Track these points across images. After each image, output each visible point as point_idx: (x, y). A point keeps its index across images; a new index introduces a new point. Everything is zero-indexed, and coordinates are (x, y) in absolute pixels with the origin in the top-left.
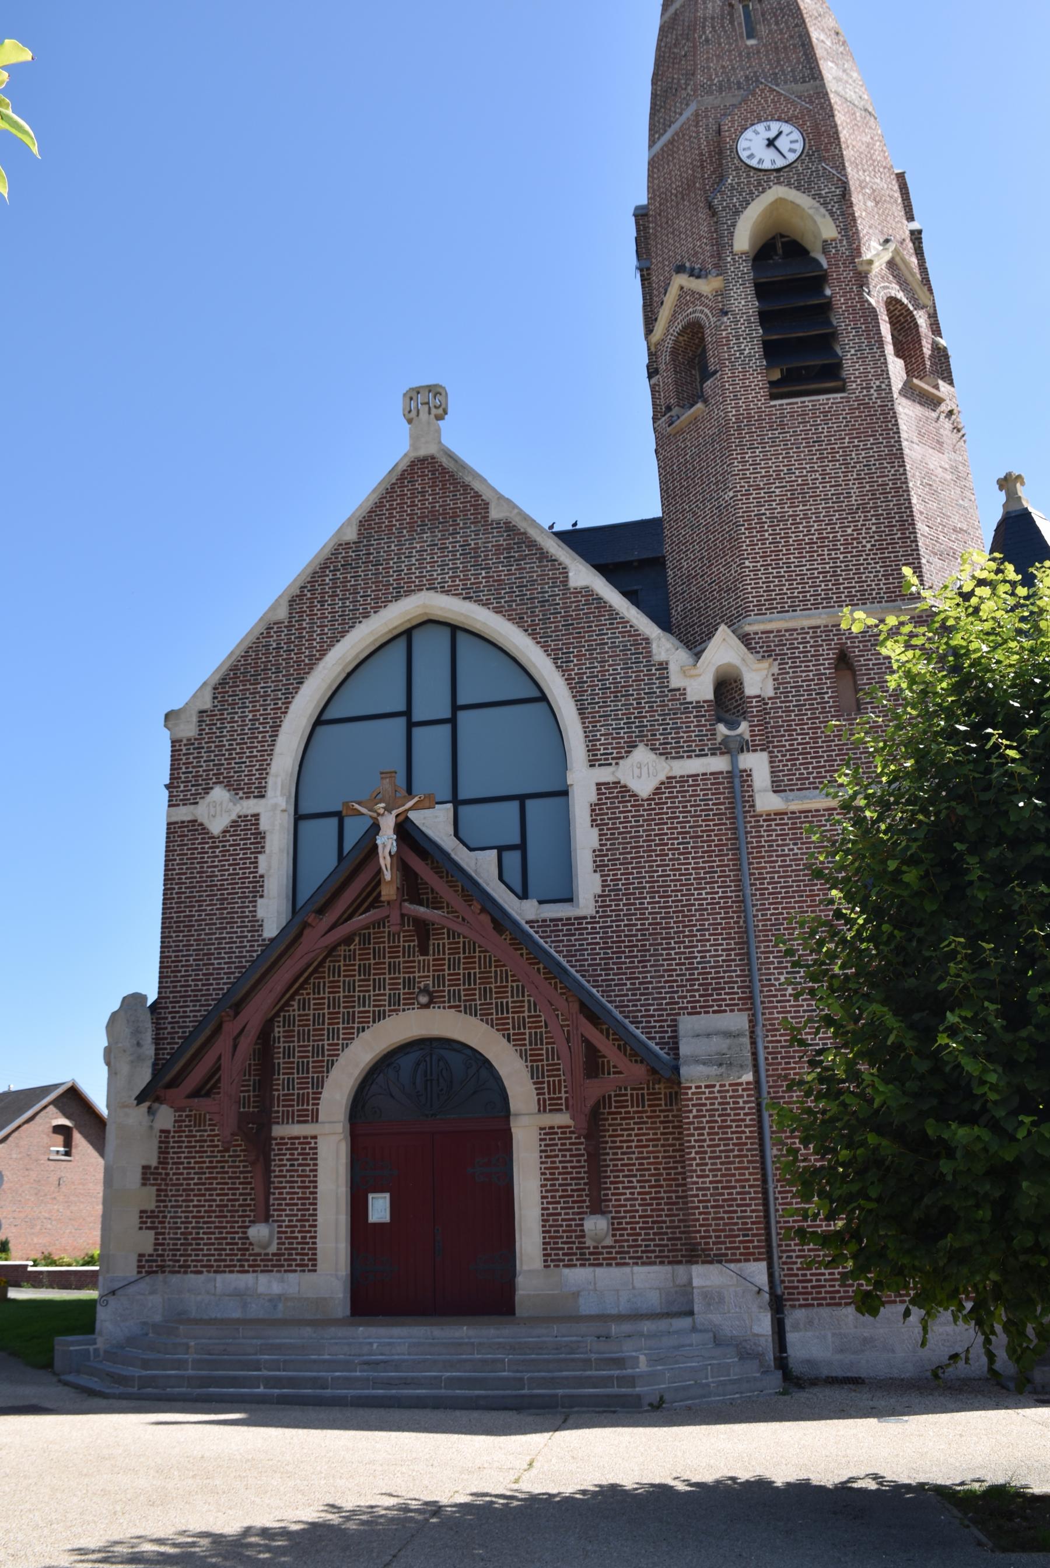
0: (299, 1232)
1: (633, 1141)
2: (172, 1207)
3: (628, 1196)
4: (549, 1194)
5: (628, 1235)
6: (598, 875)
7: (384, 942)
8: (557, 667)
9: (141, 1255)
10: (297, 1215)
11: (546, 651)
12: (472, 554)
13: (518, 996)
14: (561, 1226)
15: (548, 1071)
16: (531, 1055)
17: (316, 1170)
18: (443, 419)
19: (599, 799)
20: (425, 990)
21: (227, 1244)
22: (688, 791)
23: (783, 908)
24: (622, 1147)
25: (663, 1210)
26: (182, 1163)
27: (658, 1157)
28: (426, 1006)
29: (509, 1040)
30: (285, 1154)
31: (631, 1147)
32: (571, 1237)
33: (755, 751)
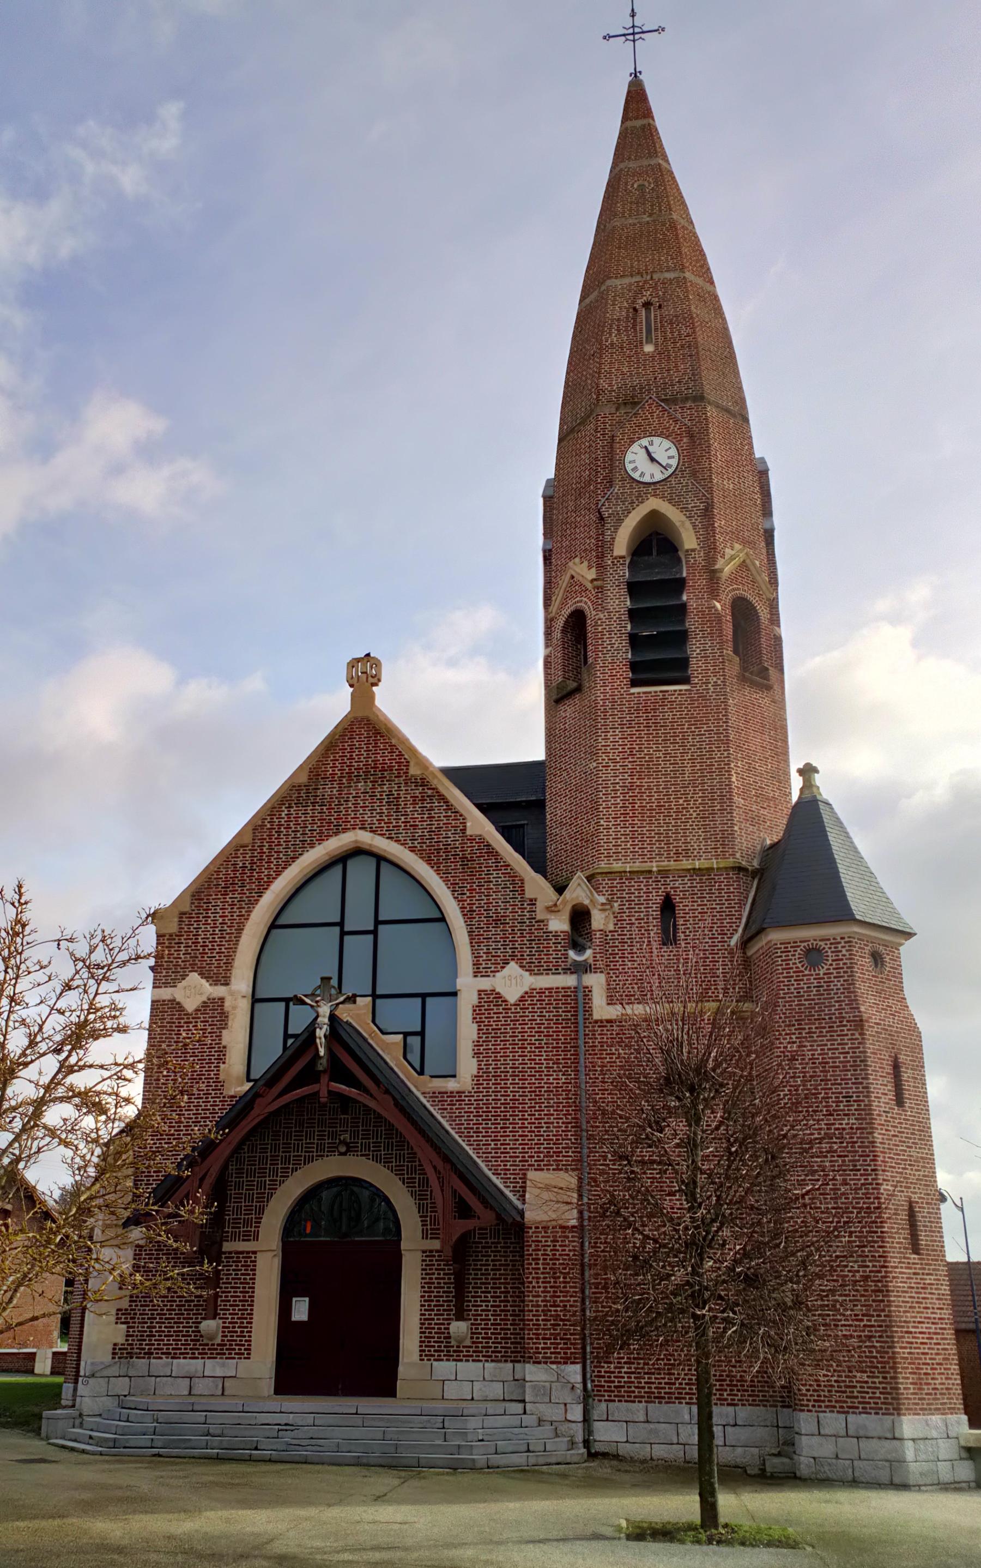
5: (483, 1338)
6: (475, 1060)
9: (115, 1345)
12: (394, 802)
18: (376, 685)
28: (344, 1154)
33: (595, 972)
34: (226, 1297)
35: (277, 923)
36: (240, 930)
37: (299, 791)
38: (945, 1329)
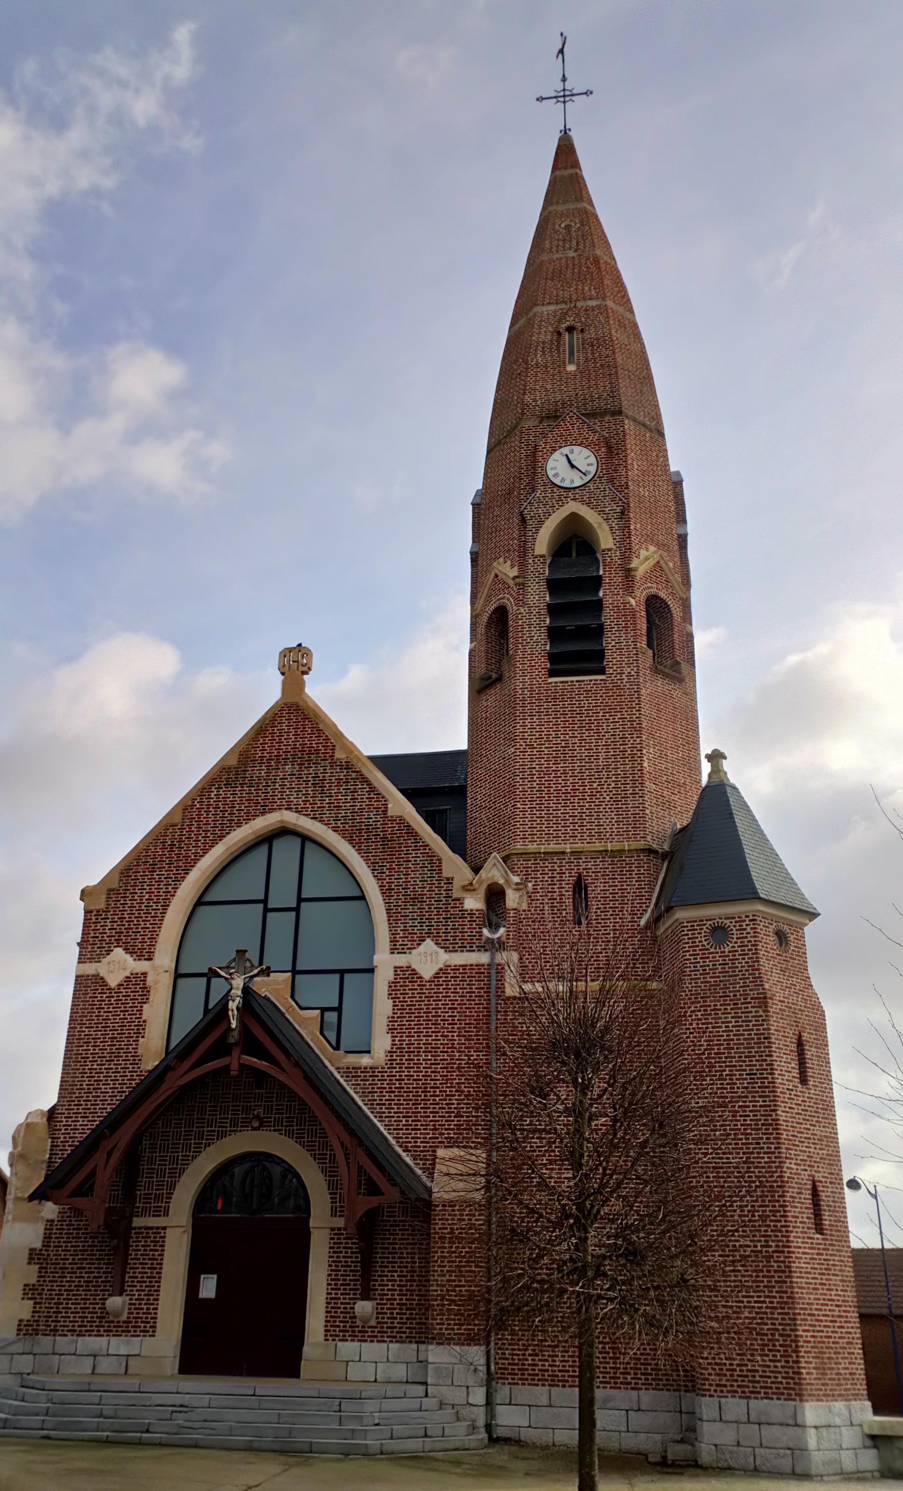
0: (145, 1304)
2: (50, 1281)
3: (390, 1287)
6: (389, 1035)
8: (375, 876)
9: (20, 1321)
12: (319, 784)
16: (330, 1172)
17: (163, 1255)
19: (396, 979)
20: (257, 1117)
26: (61, 1246)
28: (257, 1129)
36: (166, 907)
38: (848, 1312)
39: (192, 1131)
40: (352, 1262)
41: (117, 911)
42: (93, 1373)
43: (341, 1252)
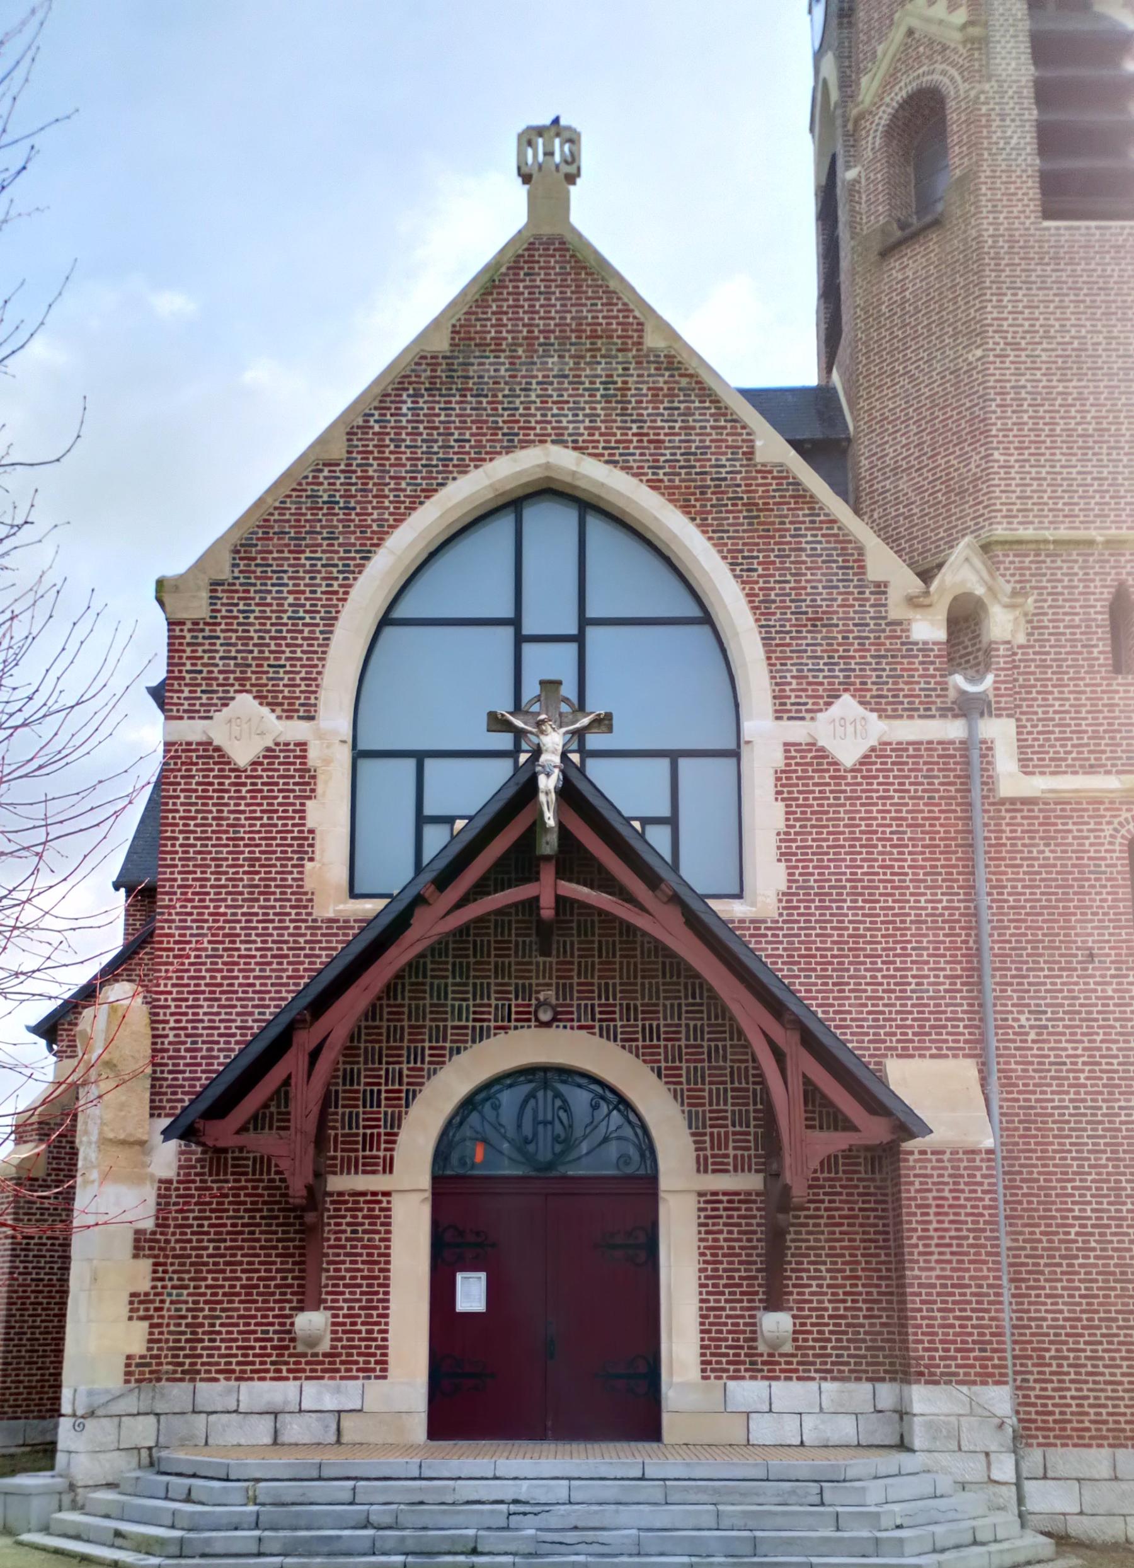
0: (363, 1324)
1: (821, 1217)
2: (173, 1287)
3: (814, 1289)
4: (710, 1282)
5: (814, 1340)
6: (783, 864)
7: (488, 935)
8: (735, 576)
9: (129, 1357)
10: (360, 1301)
11: (720, 552)
12: (617, 396)
13: (672, 1018)
14: (726, 1324)
15: (711, 1119)
16: (689, 1097)
17: (388, 1240)
19: (787, 765)
21: (256, 1340)
22: (907, 763)
23: (1027, 928)
24: (807, 1225)
25: (860, 1309)
27: (854, 1240)
28: (547, 1025)
29: (659, 1076)
30: (344, 1217)
31: (819, 1225)
32: (738, 1340)
33: (999, 716)
34: (337, 1270)
35: (397, 614)
36: (331, 620)
37: (434, 366)
39: (424, 1027)
40: (741, 1248)
41: (238, 618)
42: (275, 1442)
43: (721, 1232)
